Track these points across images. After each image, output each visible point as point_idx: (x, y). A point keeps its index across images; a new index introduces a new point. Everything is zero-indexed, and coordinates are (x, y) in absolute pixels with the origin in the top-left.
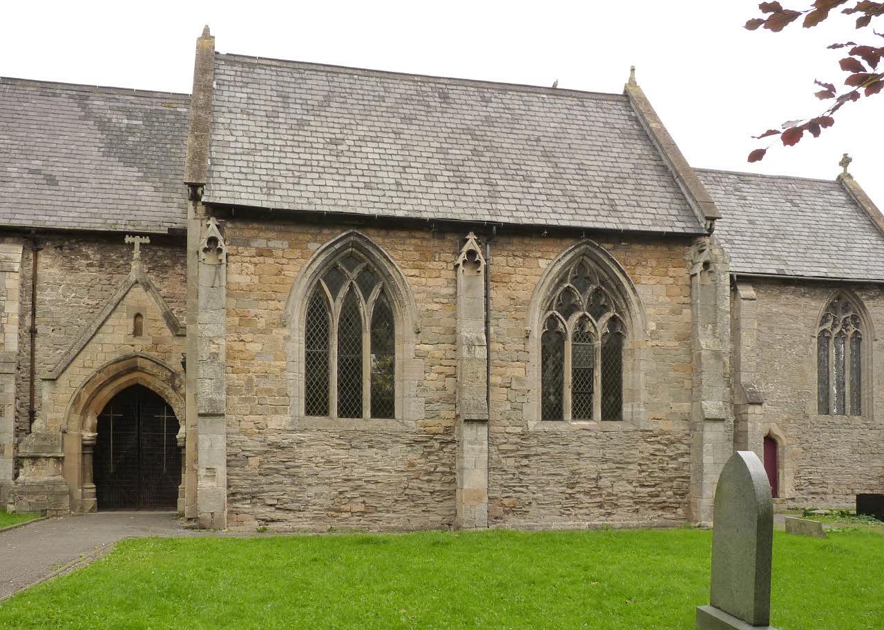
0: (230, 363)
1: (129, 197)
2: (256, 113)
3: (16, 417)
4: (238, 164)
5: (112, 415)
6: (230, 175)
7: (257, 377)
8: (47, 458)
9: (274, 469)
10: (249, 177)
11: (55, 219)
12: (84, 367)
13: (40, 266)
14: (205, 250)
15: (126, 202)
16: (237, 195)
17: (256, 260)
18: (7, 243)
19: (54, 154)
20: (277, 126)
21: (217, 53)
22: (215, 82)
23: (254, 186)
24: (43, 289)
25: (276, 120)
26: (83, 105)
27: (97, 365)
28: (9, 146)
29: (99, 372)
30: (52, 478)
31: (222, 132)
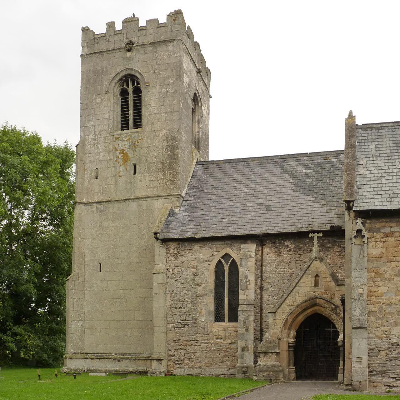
0: (370, 298)
1: (308, 212)
2: (381, 155)
3: (254, 332)
4: (372, 186)
5: (303, 330)
6: (368, 193)
7: (385, 306)
8: (271, 353)
9: (395, 357)
10: (379, 193)
11: (271, 228)
12: (289, 305)
13: (264, 254)
14: (355, 237)
15: (307, 215)
16: (373, 204)
17: (384, 239)
18: (249, 243)
19: (270, 194)
20: (394, 161)
21: (357, 125)
22: (356, 142)
23: (382, 198)
24: (266, 266)
25: (393, 158)
26: (282, 166)
27: (296, 304)
28: (247, 193)
29: (297, 307)
30: (274, 363)
31: (362, 169)
